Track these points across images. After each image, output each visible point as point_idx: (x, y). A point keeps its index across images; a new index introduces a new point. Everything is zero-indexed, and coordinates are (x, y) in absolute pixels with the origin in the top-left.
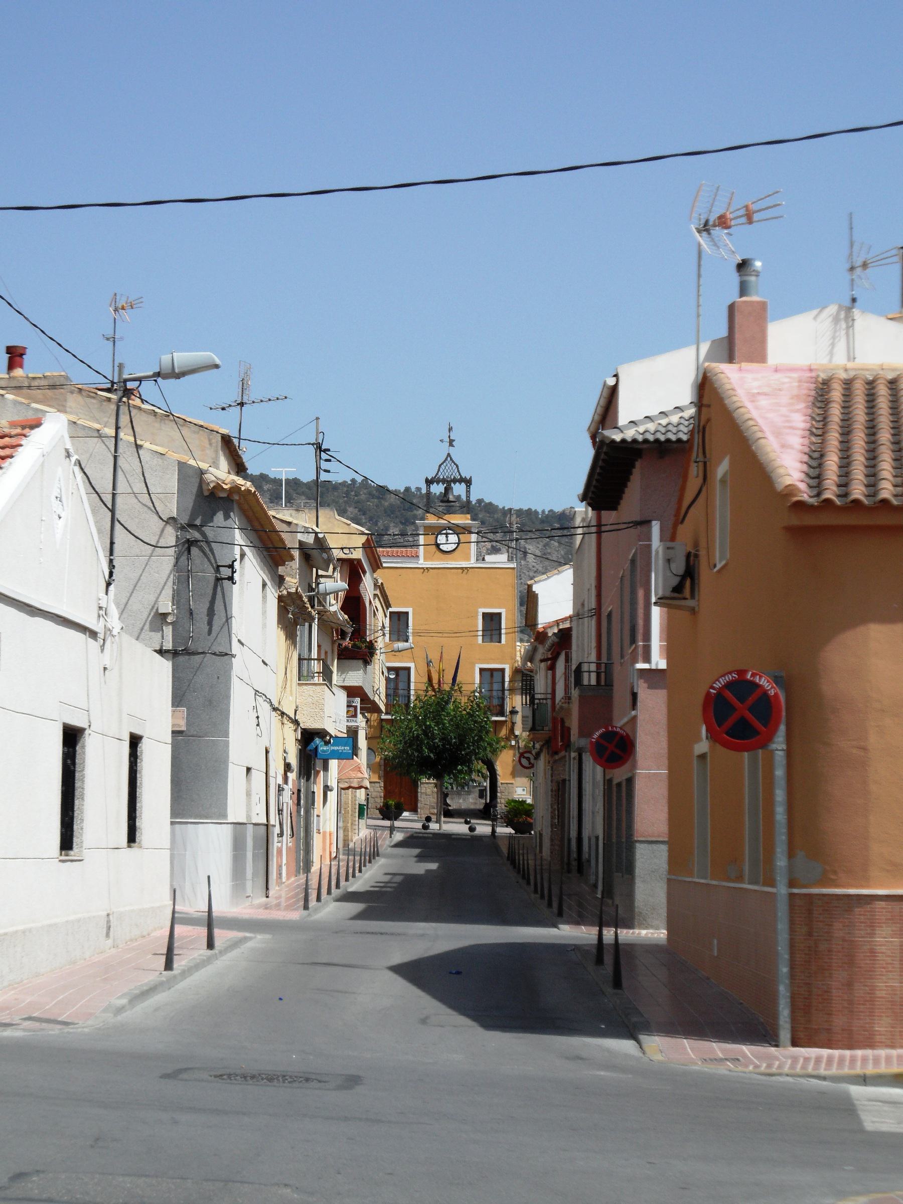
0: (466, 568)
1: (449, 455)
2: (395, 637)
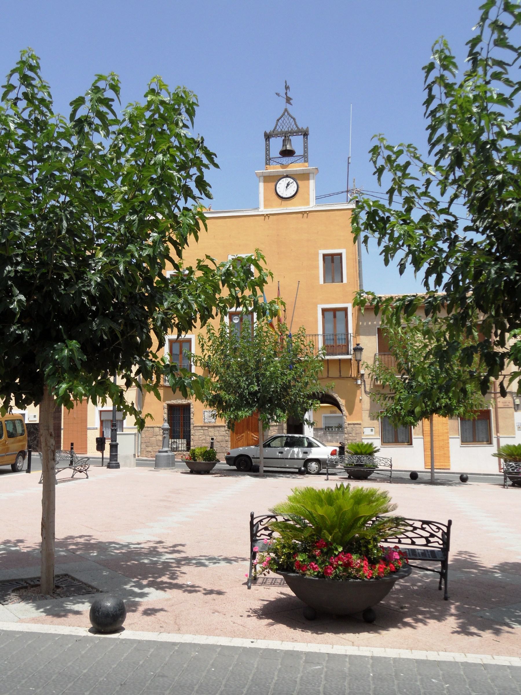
0: (305, 212)
1: (286, 110)
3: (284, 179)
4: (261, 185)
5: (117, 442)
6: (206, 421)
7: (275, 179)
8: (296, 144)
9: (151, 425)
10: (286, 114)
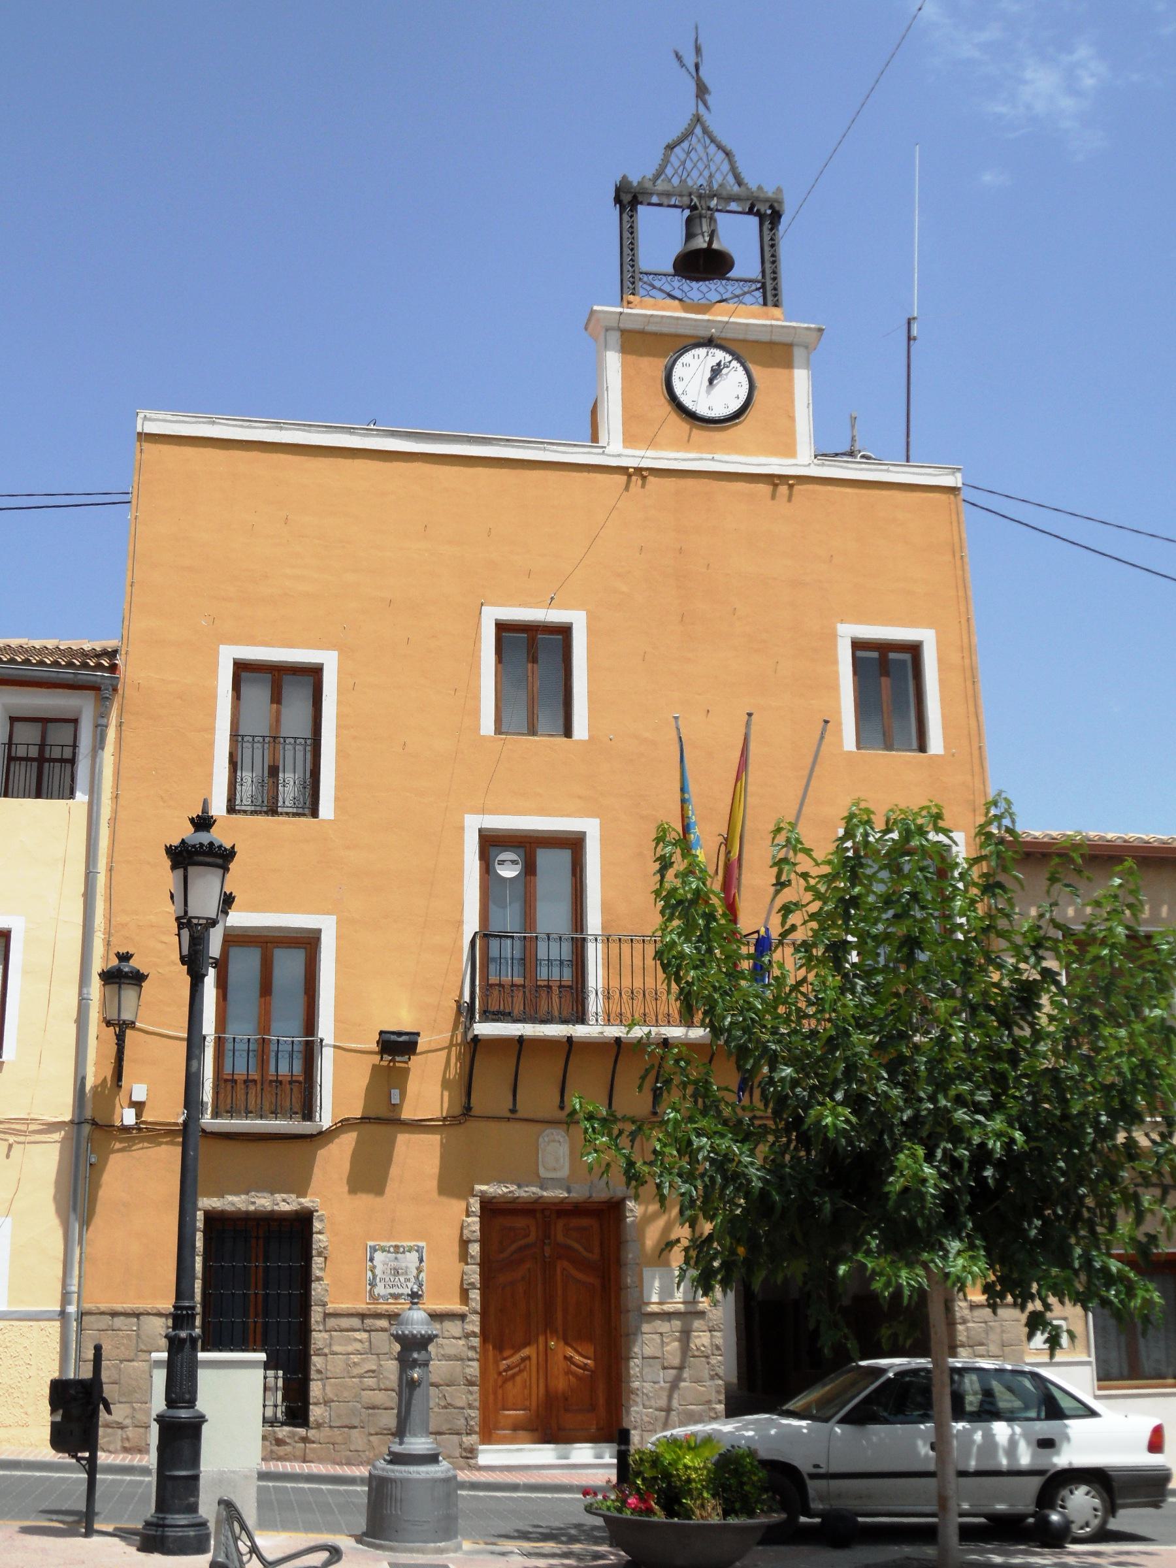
0: (784, 478)
1: (698, 119)
2: (520, 716)
3: (702, 351)
4: (613, 361)
5: (202, 1405)
6: (380, 1290)
7: (660, 346)
8: (736, 235)
9: (128, 1306)
10: (698, 130)
